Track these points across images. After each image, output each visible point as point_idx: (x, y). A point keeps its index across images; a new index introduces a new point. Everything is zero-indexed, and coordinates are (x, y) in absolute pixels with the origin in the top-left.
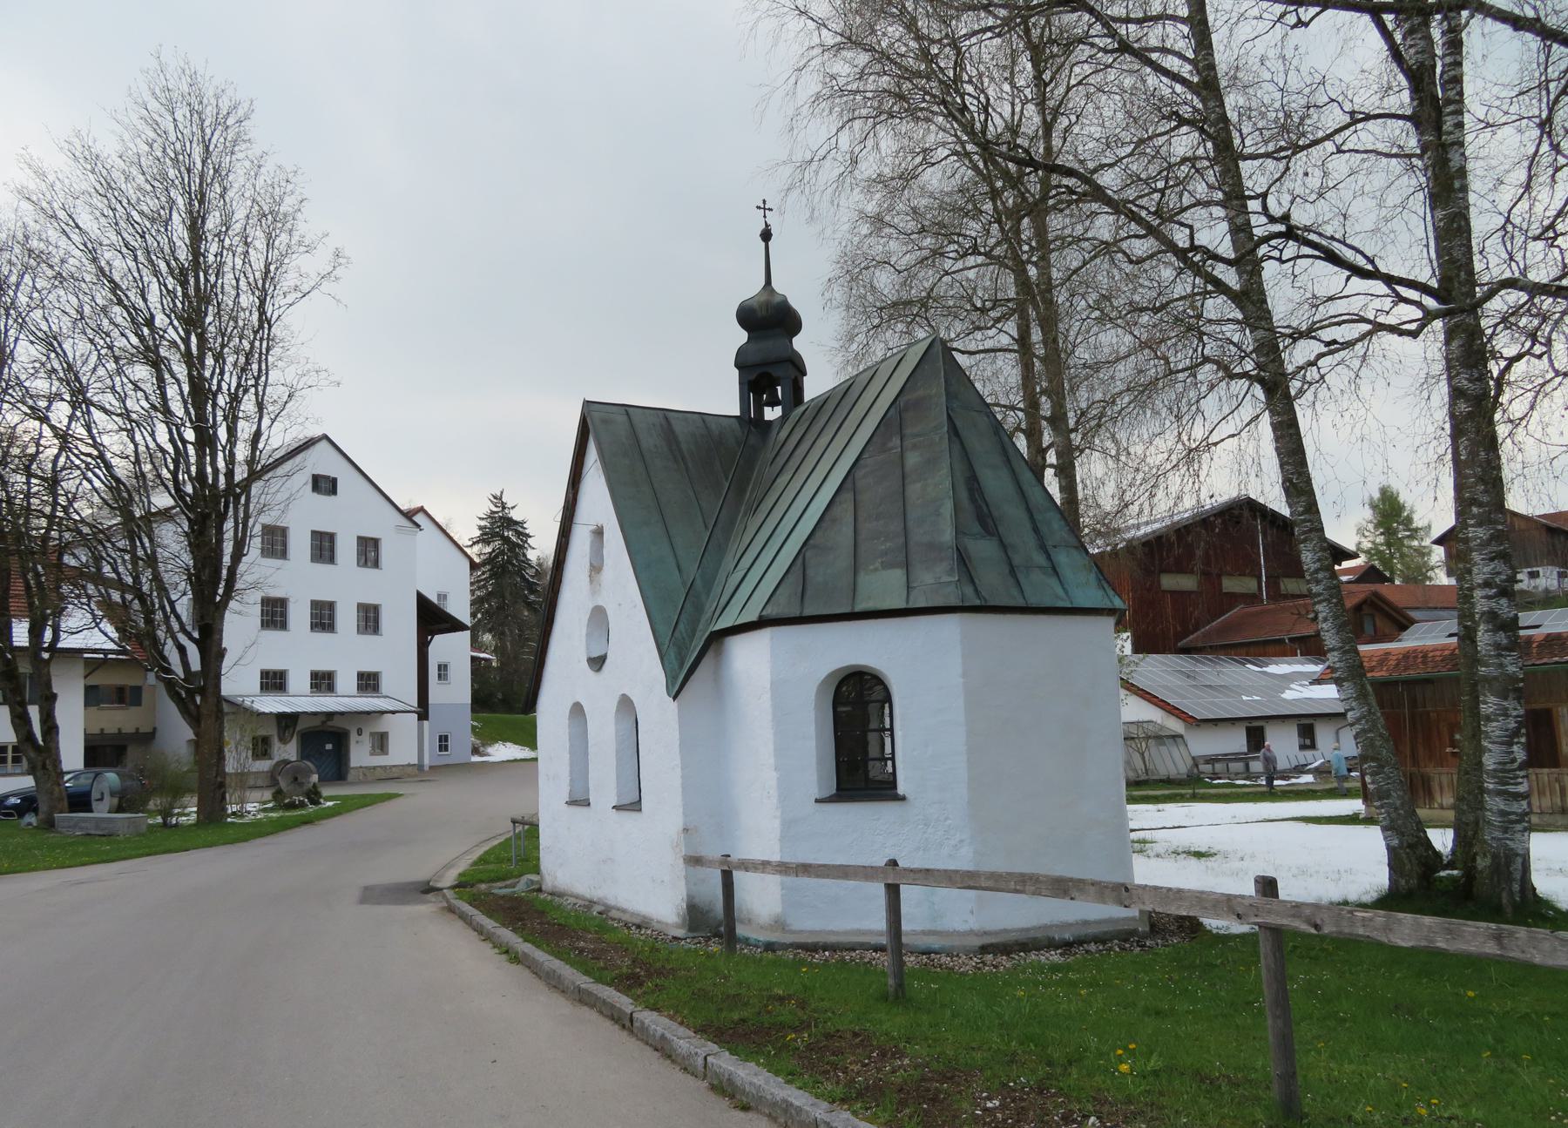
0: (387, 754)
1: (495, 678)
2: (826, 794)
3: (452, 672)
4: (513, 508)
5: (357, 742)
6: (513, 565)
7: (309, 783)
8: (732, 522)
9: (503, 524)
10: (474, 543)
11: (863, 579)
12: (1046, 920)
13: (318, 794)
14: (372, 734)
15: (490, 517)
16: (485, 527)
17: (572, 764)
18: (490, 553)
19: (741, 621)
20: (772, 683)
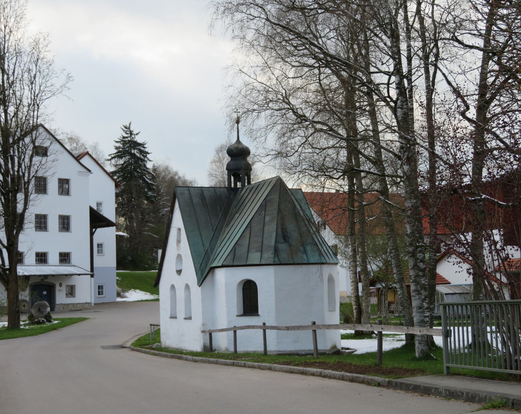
0: (74, 297)
1: (126, 246)
2: (240, 314)
3: (105, 248)
4: (137, 134)
5: (59, 290)
6: (138, 172)
7: (46, 311)
8: (222, 228)
9: (130, 145)
10: (112, 158)
11: (250, 255)
12: (298, 349)
13: (50, 317)
14: (67, 286)
15: (122, 141)
16: (119, 147)
17: (171, 305)
18: (123, 164)
19: (217, 265)
20: (225, 283)
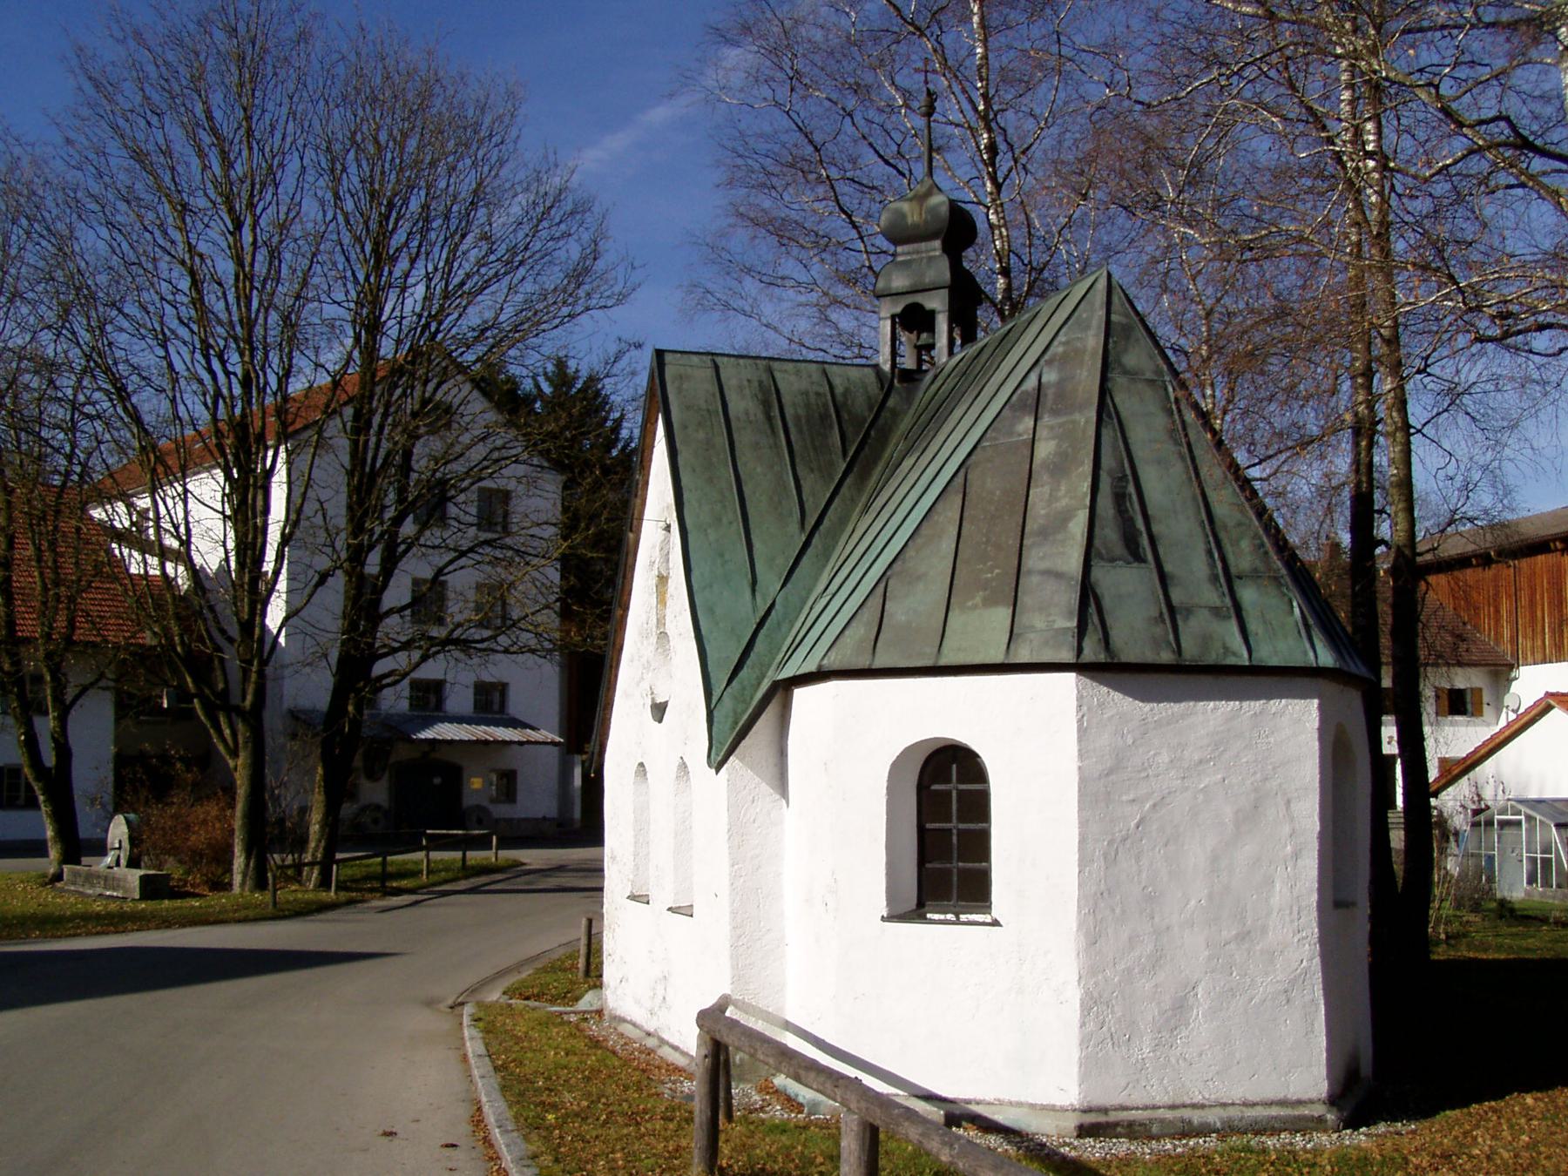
19: (801, 671)
